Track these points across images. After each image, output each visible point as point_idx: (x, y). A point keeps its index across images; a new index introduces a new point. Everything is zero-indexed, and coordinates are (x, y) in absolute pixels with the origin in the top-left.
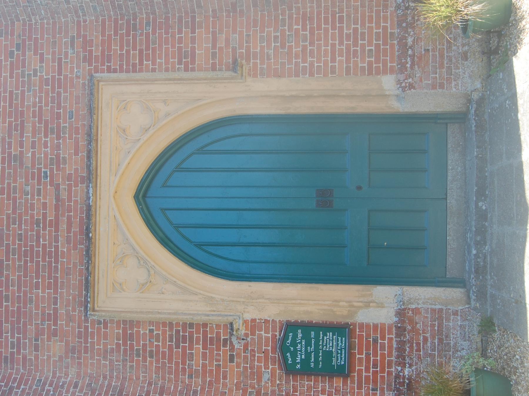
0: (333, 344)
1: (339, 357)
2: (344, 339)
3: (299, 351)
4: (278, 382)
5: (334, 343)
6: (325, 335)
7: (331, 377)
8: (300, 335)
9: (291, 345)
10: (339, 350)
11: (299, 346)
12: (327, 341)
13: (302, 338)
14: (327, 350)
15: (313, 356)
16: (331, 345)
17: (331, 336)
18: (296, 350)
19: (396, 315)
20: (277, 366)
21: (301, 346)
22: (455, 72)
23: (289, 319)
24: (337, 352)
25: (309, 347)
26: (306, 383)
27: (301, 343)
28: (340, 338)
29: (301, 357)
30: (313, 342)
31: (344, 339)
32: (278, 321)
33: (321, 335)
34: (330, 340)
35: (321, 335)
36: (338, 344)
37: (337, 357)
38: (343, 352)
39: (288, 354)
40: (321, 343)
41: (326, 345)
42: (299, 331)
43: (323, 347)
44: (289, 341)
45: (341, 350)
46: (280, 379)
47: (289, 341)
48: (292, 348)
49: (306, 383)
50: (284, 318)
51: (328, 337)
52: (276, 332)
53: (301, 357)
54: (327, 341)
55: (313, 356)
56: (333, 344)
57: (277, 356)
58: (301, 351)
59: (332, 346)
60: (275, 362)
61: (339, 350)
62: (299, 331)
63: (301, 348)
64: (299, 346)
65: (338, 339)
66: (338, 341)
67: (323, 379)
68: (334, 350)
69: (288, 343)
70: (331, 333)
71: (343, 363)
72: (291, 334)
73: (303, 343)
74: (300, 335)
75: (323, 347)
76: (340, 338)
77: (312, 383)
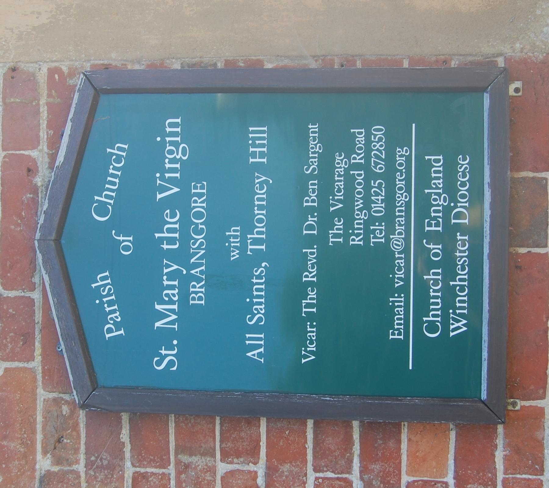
0: (390, 200)
1: (435, 292)
2: (464, 164)
3: (172, 256)
4: (44, 464)
5: (401, 198)
6: (338, 141)
7: (382, 428)
8: (176, 155)
9: (119, 223)
10: (433, 237)
11: (173, 221)
12: (350, 180)
13: (190, 172)
14: (357, 241)
15: (259, 285)
16: (378, 206)
17: (378, 146)
18: (150, 254)
19: (497, 445)
20: (36, 364)
21: (185, 223)
22: (512, 178)
23: (114, 58)
24: (421, 251)
25: (234, 231)
26: (222, 468)
27: (181, 203)
28: (437, 163)
29: (184, 295)
30: (261, 193)
31: (464, 164)
32: (42, 77)
33: (315, 147)
34: (370, 176)
35: (315, 147)
36: (424, 206)
37: (422, 289)
38: (462, 253)
39: (103, 281)
40: (311, 200)
41: (347, 214)
42: (173, 125)
43: (326, 223)
44: (107, 197)
45: (447, 236)
46: (56, 445)
47: (107, 197)
48: (126, 240)
49: (222, 468)
50: (78, 58)
51: (358, 159)
52: (34, 144)
53: (184, 295)
54: (350, 180)
55: (259, 285)
56: (390, 200)
57: (36, 295)
58: (182, 256)
59: (389, 219)
60: (27, 338)
61: (433, 237)
62: (173, 125)
63: (185, 239)
64: (173, 221)
65: (424, 169)
66: (424, 180)
67: (331, 442)
68: (397, 242)
69: (102, 209)
70: (379, 132)
71: (458, 327)
72: (119, 150)
73: (199, 205)
74: (176, 155)
75: (326, 223)
76: (437, 163)
77: (260, 469)
